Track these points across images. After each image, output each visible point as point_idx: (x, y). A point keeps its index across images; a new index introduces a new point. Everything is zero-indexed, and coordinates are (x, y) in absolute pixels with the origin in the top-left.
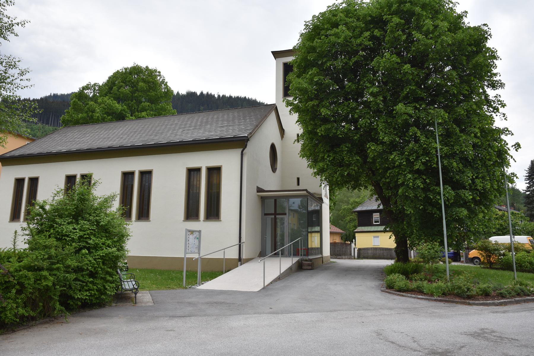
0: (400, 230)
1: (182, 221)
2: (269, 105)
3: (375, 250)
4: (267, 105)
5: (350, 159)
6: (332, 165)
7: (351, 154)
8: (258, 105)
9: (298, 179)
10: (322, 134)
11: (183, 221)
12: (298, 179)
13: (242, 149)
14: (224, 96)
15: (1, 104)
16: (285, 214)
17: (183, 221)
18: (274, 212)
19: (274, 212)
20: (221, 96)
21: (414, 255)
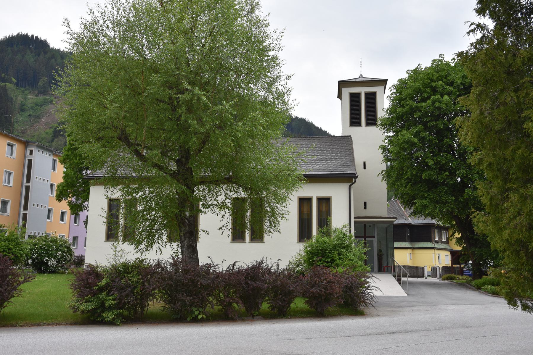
0: (484, 253)
1: (296, 243)
2: (337, 137)
3: (398, 268)
4: (334, 137)
5: (447, 199)
6: (431, 202)
7: (447, 194)
8: (328, 135)
9: (365, 203)
10: (425, 179)
11: (297, 243)
12: (365, 203)
13: (351, 183)
14: (37, 38)
15: (532, 229)
16: (374, 237)
17: (297, 243)
18: (363, 235)
19: (363, 235)
20: (35, 37)
21: (440, 273)
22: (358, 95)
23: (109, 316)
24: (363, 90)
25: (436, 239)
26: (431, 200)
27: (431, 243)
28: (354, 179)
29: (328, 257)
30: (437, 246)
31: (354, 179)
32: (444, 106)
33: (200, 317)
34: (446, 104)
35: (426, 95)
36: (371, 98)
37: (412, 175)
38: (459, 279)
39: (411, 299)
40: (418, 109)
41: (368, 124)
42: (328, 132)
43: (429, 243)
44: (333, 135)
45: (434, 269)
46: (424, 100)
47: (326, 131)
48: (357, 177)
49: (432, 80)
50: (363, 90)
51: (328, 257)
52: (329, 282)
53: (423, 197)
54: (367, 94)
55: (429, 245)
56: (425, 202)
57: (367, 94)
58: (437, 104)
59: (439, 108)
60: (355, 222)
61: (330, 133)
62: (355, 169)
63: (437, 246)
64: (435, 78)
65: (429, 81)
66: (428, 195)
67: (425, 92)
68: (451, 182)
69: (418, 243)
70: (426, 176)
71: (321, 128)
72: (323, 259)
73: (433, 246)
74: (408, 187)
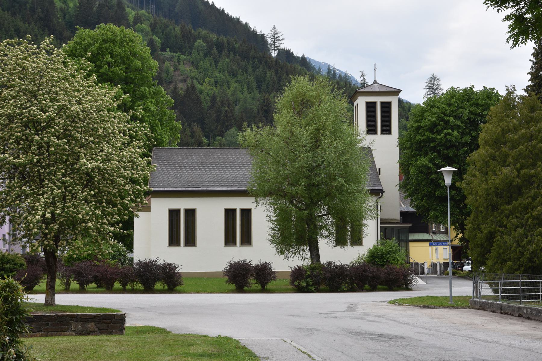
21: (440, 269)
22: (374, 104)
23: (312, 288)
24: (378, 100)
25: (434, 229)
26: (441, 212)
27: (428, 234)
28: (381, 194)
29: (385, 259)
30: (435, 237)
31: (381, 194)
32: (454, 139)
33: (345, 289)
34: (455, 138)
35: (440, 128)
36: (386, 107)
37: (428, 191)
38: (460, 274)
39: (428, 285)
40: (434, 140)
41: (383, 133)
42: (226, 12)
43: (426, 234)
44: (235, 17)
45: (434, 265)
46: (439, 132)
47: (223, 10)
48: (384, 192)
49: (445, 115)
50: (378, 100)
51: (385, 259)
52: (398, 272)
53: (436, 210)
54: (382, 104)
55: (426, 236)
56: (437, 214)
57: (382, 104)
58: (448, 137)
59: (450, 141)
60: (381, 227)
61: (230, 14)
62: (381, 185)
63: (435, 237)
64: (447, 113)
65: (443, 115)
66: (440, 208)
67: (439, 125)
68: (457, 198)
69: (413, 234)
70: (438, 193)
71: (213, 4)
72: (382, 260)
73: (430, 238)
74: (424, 201)
